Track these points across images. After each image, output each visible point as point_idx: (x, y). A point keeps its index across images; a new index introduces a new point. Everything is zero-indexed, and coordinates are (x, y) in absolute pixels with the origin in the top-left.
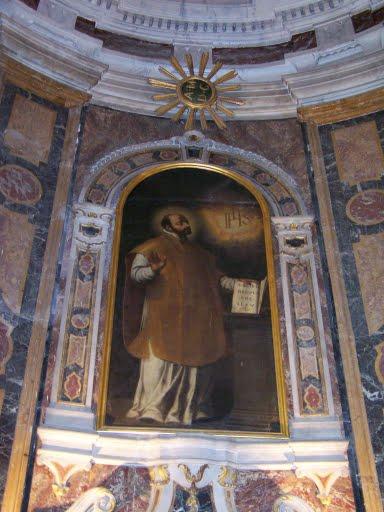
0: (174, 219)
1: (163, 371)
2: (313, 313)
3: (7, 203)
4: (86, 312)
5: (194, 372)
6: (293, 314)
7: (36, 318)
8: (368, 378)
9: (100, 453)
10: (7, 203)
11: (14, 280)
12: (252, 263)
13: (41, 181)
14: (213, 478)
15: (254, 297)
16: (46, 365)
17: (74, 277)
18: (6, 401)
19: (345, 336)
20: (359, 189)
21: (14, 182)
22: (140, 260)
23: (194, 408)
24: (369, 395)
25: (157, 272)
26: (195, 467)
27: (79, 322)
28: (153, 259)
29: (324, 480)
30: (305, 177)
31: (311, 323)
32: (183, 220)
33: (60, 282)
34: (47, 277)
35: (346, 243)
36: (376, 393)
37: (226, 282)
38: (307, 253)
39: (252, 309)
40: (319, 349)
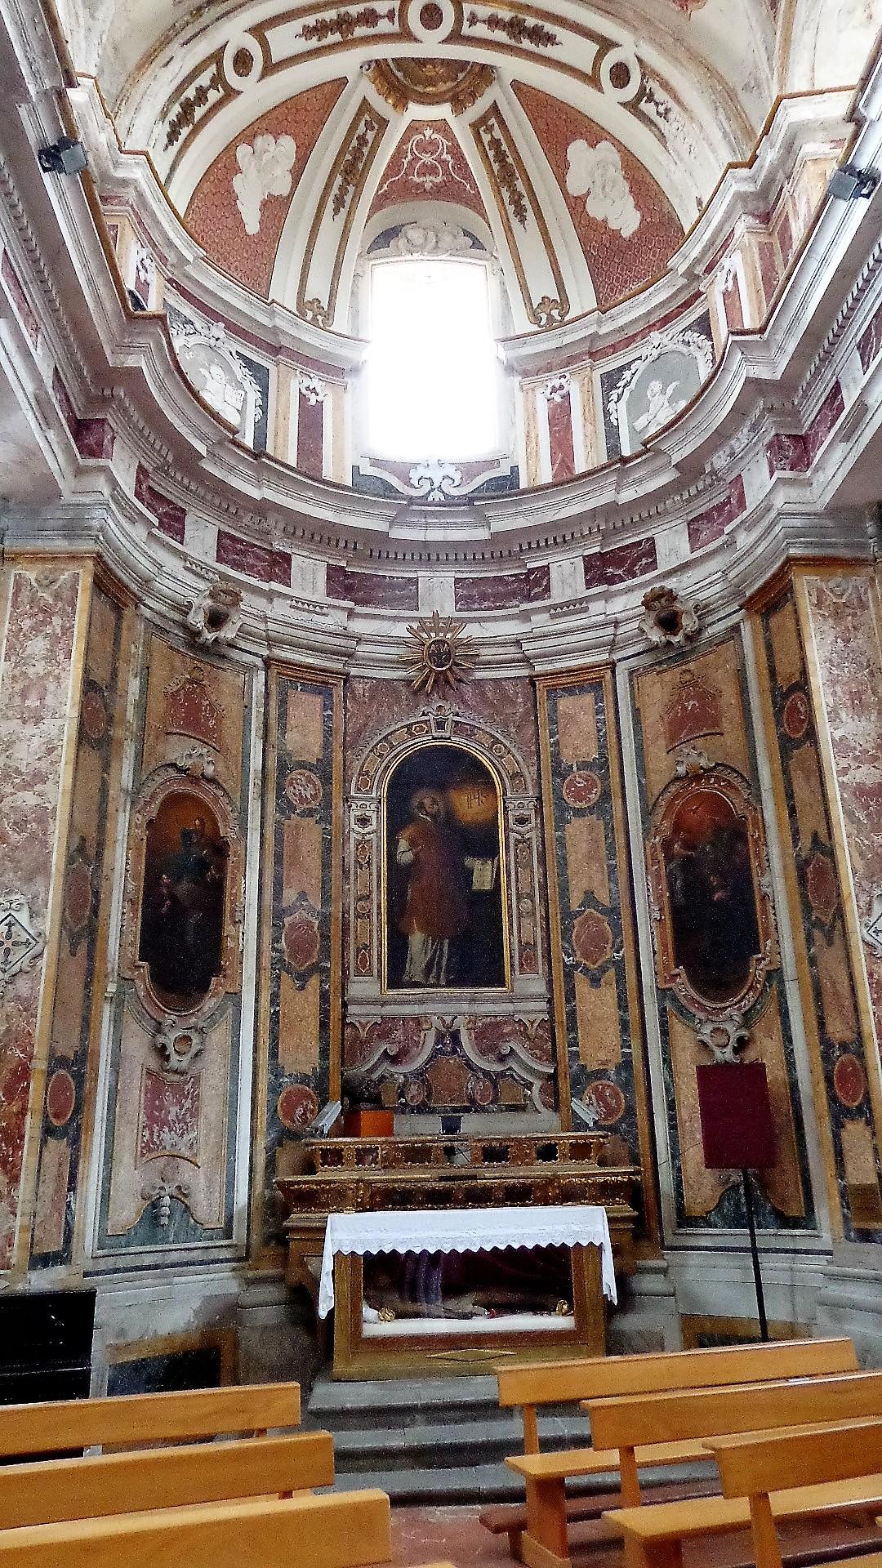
0: (427, 802)
1: (425, 942)
2: (533, 888)
3: (298, 811)
4: (368, 897)
5: (447, 941)
6: (517, 889)
7: (332, 909)
8: (566, 945)
9: (555, 296)
10: (298, 811)
11: (313, 881)
12: (483, 842)
13: (320, 779)
14: (461, 1023)
15: (490, 873)
16: (344, 946)
17: (355, 867)
18: (321, 982)
19: (554, 910)
20: (575, 769)
21: (300, 788)
22: (403, 845)
23: (448, 972)
24: (566, 959)
25: (416, 855)
26: (448, 1019)
27: (364, 909)
28: (413, 843)
29: (532, 1023)
30: (533, 748)
31: (531, 897)
32: (434, 802)
33: (346, 873)
34: (336, 872)
35: (561, 823)
36: (571, 958)
37: (468, 861)
38: (531, 832)
39: (487, 887)
40: (535, 921)
